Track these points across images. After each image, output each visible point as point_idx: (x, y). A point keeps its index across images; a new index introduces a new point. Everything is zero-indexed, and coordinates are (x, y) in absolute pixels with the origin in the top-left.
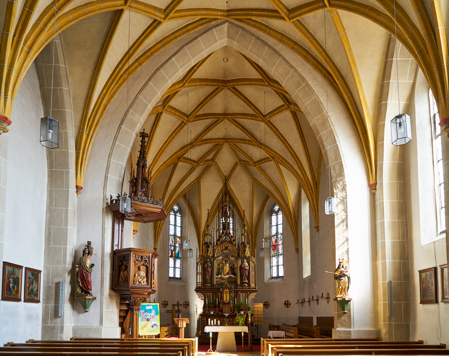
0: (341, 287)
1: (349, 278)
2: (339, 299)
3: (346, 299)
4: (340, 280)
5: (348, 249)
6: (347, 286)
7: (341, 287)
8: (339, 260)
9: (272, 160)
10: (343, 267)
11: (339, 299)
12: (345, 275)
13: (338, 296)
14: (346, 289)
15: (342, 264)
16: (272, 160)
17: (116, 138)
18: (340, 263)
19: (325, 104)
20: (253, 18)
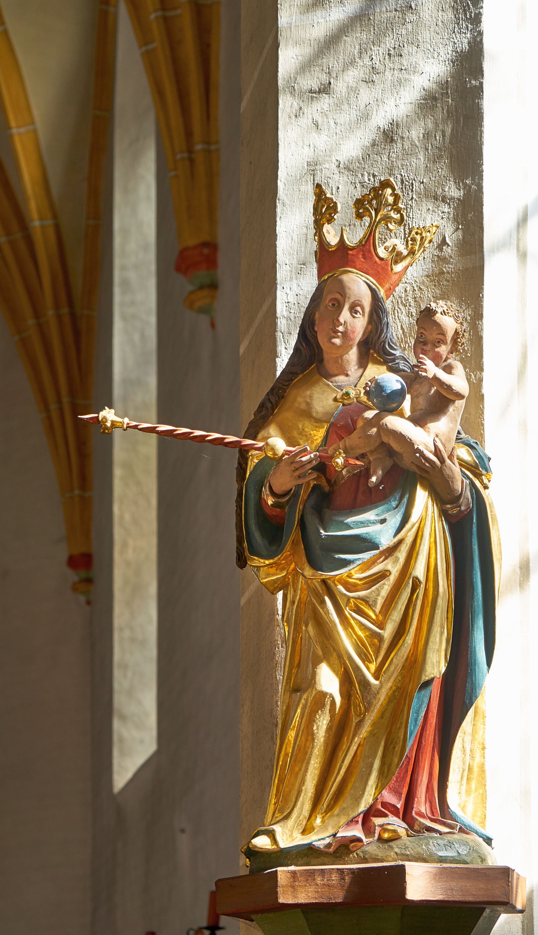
0: (328, 681)
1: (469, 530)
2: (294, 888)
3: (420, 885)
4: (322, 555)
5: (469, 63)
6: (436, 665)
7: (328, 681)
8: (324, 209)
9: (458, 458)
10: (374, 347)
11: (294, 888)
12: (403, 473)
13: (288, 836)
14: (424, 706)
15: (357, 284)
16: (458, 458)
17: (57, 228)
18: (331, 260)
19: (450, 339)
20: (377, 220)
